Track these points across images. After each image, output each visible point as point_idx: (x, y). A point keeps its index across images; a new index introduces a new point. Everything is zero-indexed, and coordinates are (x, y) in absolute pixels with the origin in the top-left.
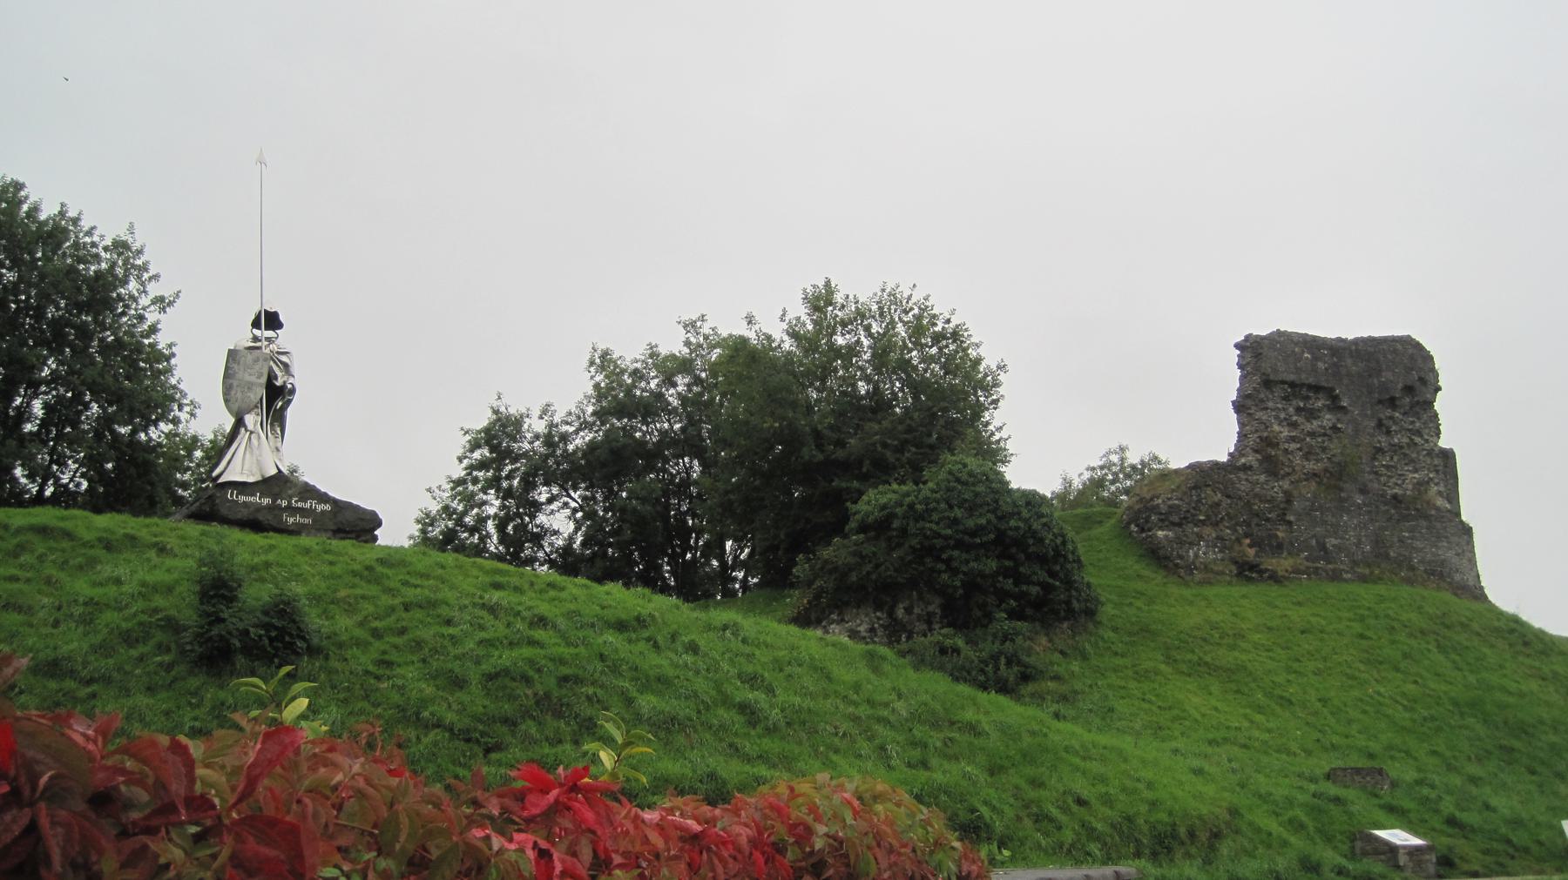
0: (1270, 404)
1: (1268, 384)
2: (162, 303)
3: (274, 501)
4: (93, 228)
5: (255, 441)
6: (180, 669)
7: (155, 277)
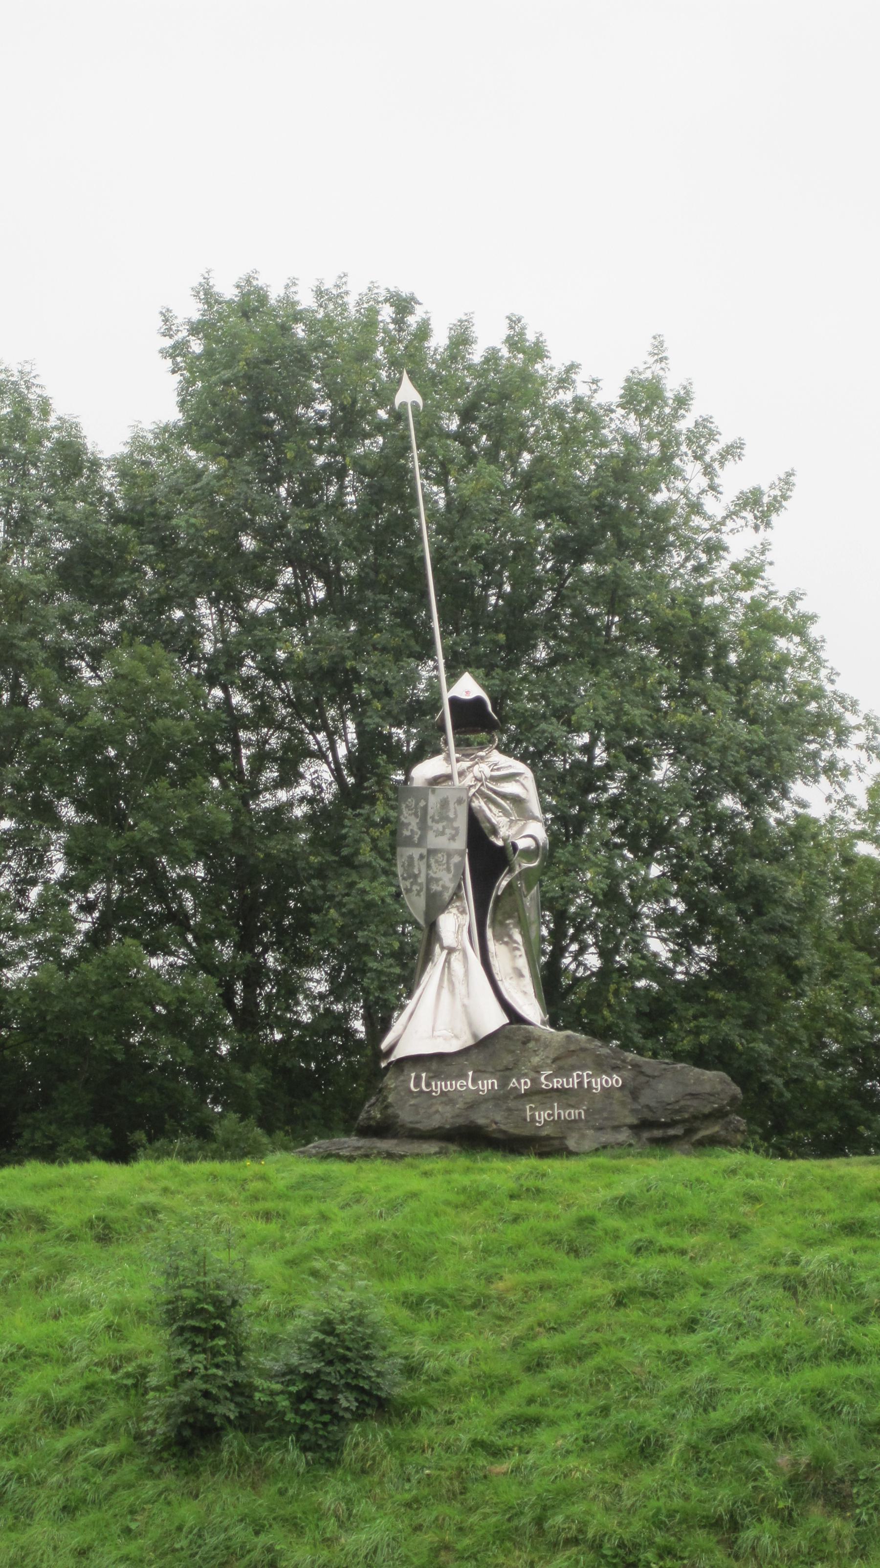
2: (758, 506)
3: (504, 1083)
4: (572, 368)
6: (127, 1471)
7: (732, 451)
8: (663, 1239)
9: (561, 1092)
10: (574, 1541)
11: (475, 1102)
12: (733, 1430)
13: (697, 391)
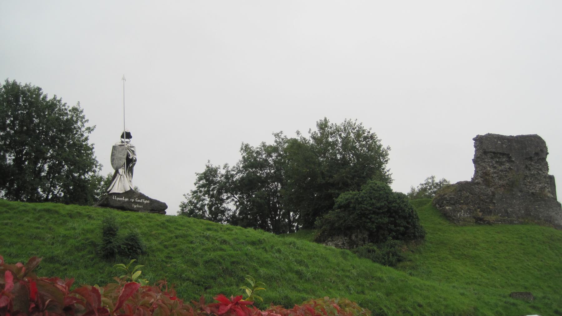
0: (486, 160)
1: (485, 153)
2: (89, 130)
4: (66, 104)
5: (122, 178)
7: (87, 121)
8: (179, 228)
9: (139, 202)
10: (188, 280)
11: (124, 202)
12: (209, 261)
13: (84, 111)
